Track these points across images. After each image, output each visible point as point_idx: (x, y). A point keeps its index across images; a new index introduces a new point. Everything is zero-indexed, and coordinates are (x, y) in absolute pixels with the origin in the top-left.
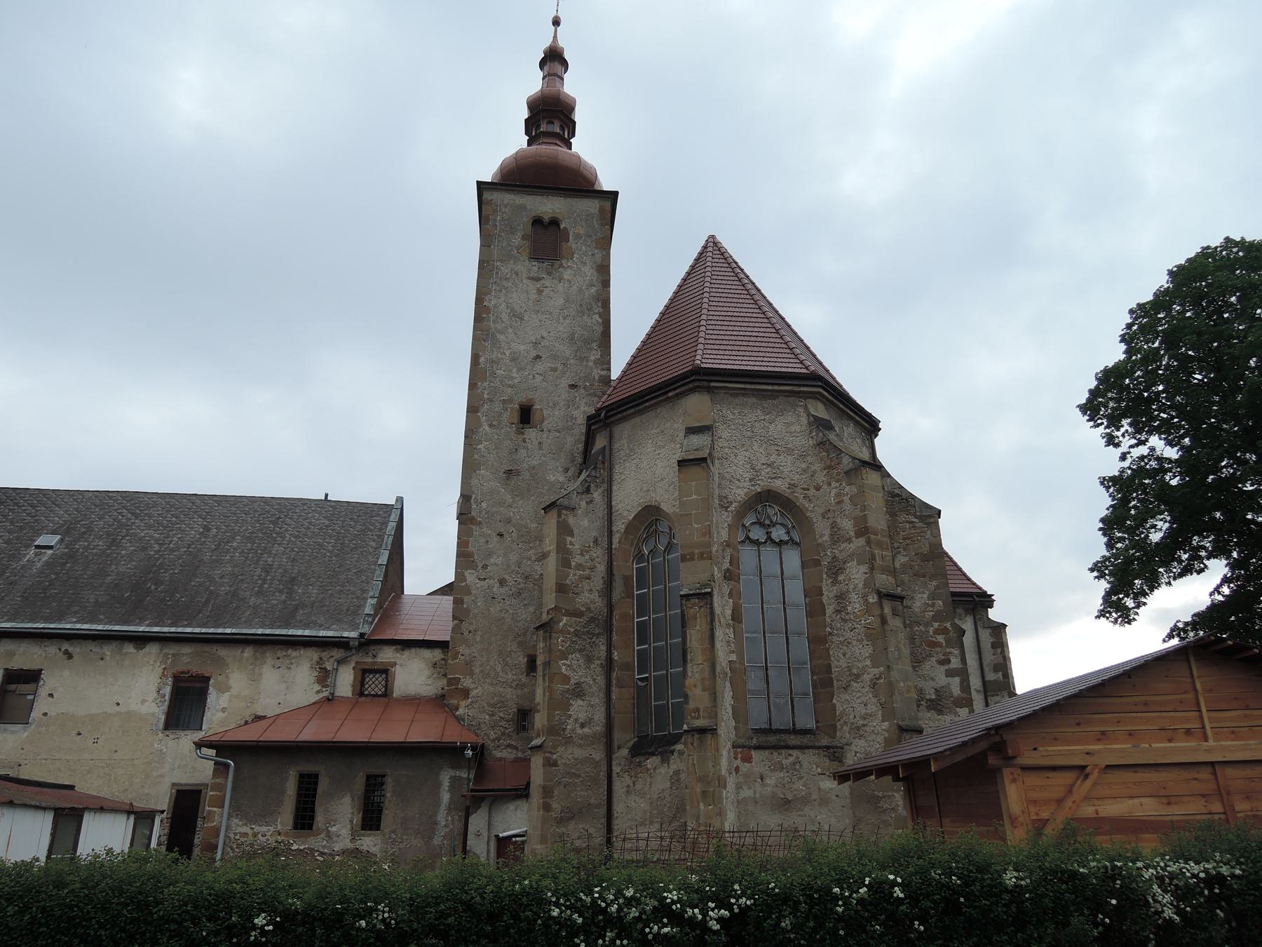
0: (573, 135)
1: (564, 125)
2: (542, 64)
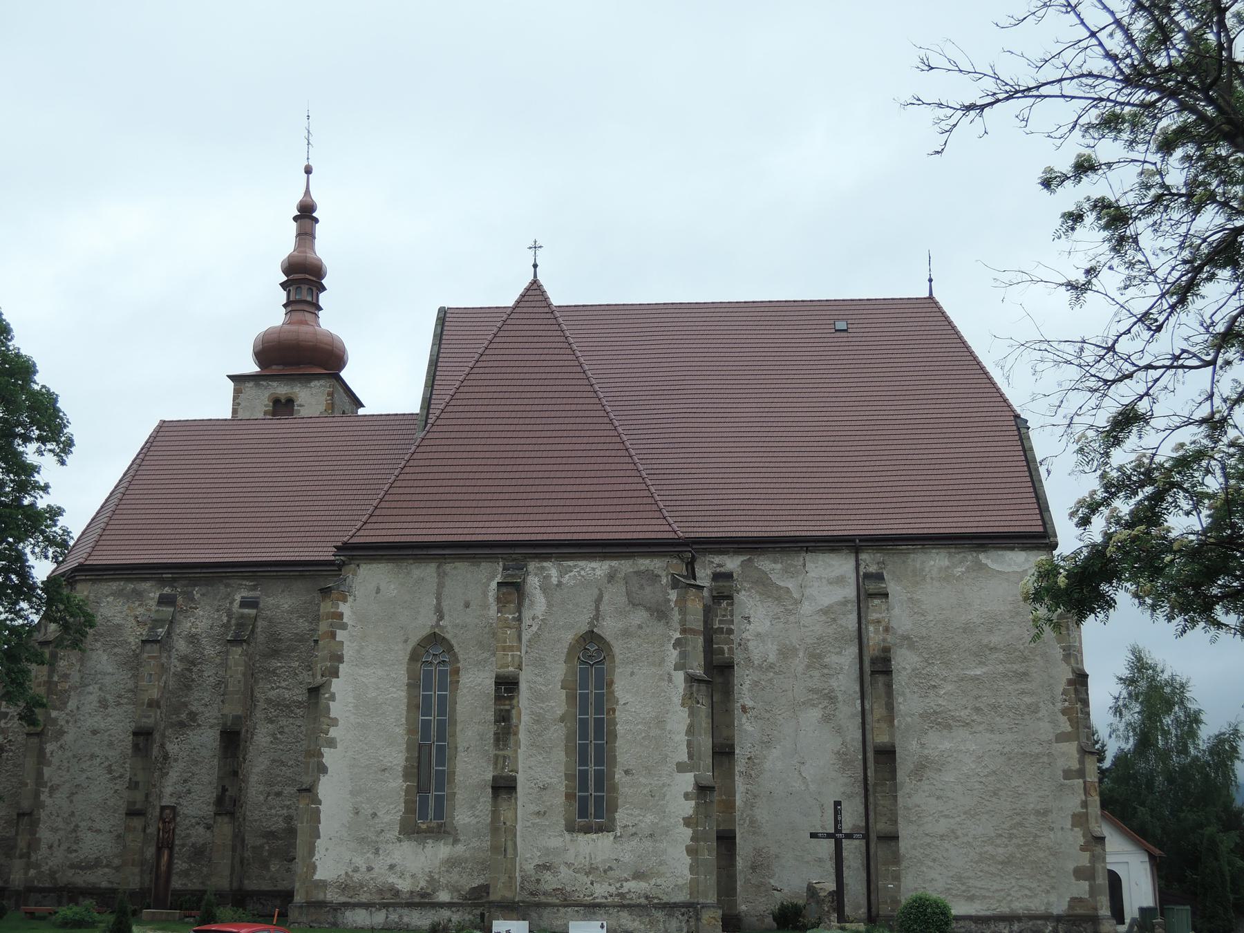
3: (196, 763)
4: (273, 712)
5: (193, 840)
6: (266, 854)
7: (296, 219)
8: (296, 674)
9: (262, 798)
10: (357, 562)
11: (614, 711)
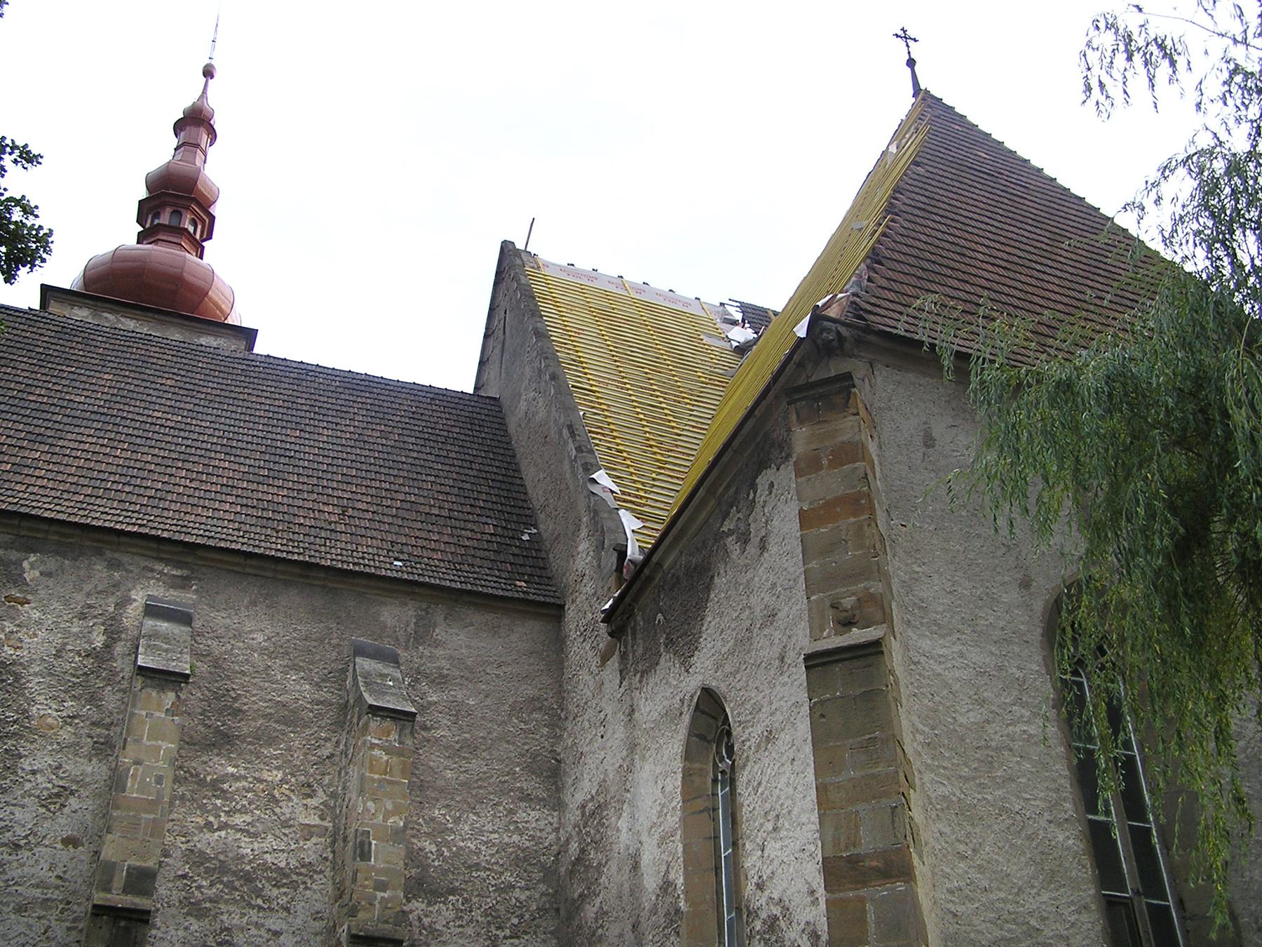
0: (210, 237)
1: (198, 221)
2: (179, 127)
4: (205, 888)
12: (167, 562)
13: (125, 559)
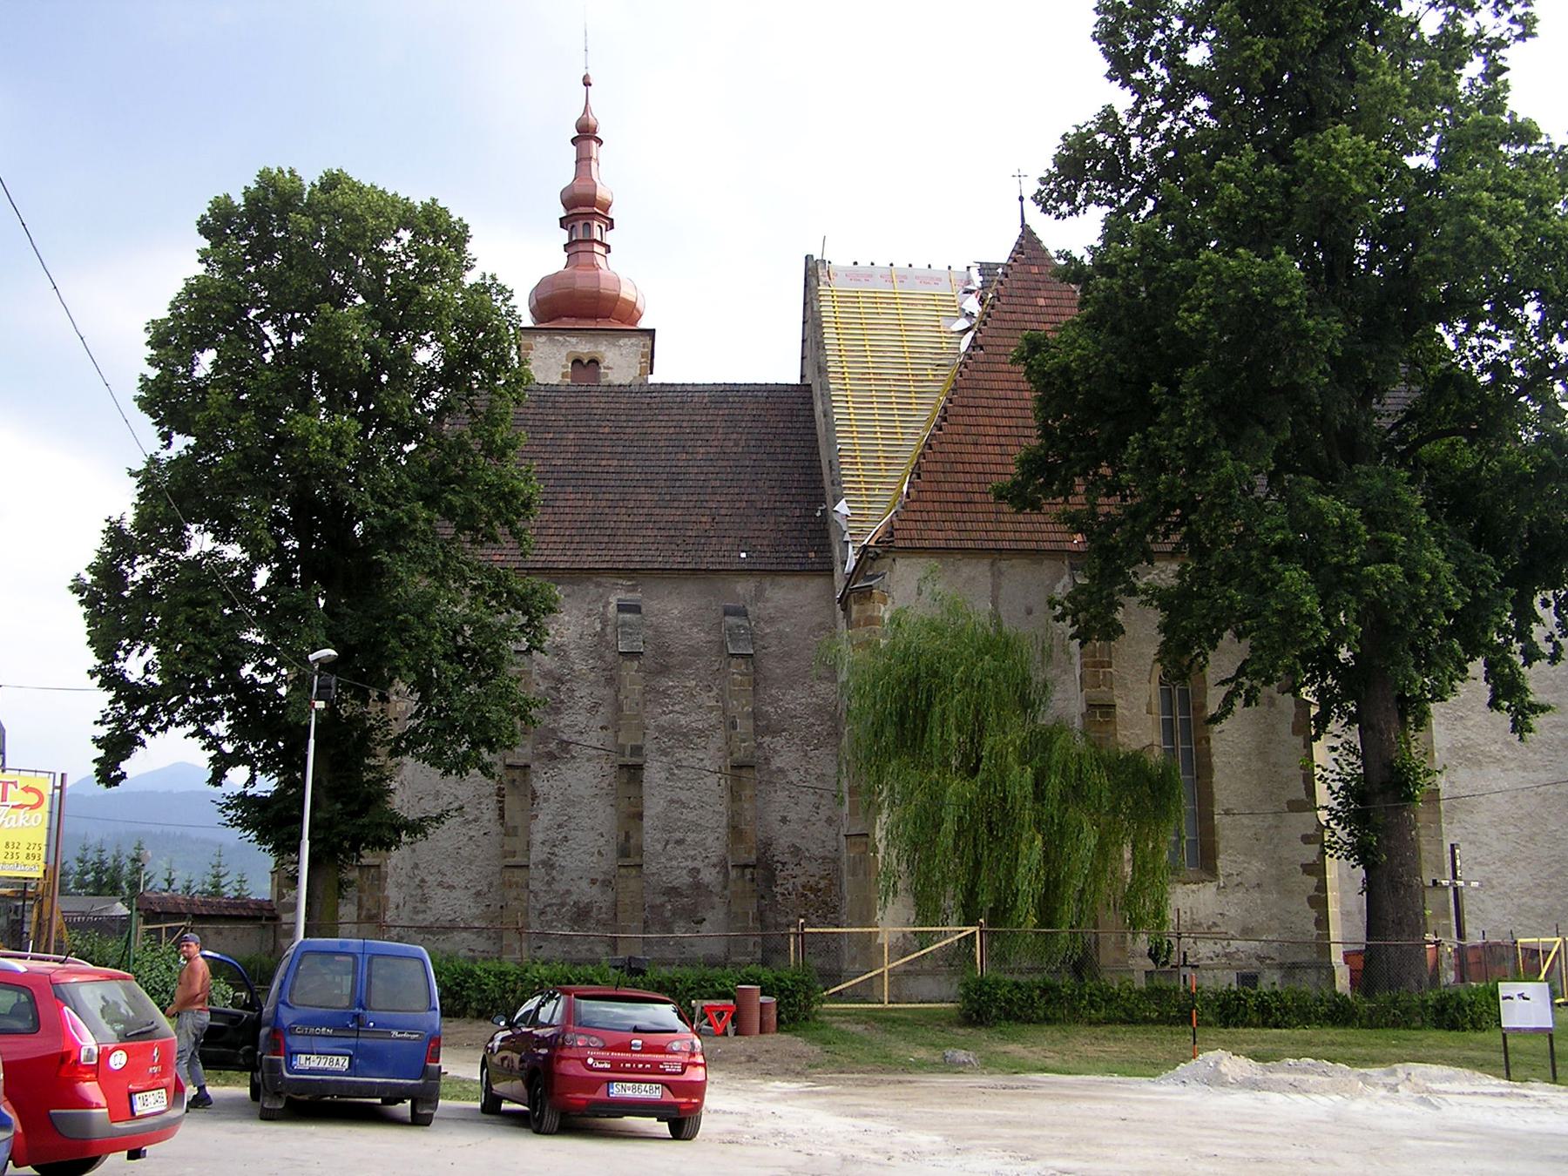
3: (573, 804)
4: (667, 742)
5: (574, 897)
6: (668, 914)
7: (574, 141)
8: (692, 695)
9: (659, 847)
10: (893, 555)
11: (1208, 741)
12: (624, 578)
13: (603, 580)
